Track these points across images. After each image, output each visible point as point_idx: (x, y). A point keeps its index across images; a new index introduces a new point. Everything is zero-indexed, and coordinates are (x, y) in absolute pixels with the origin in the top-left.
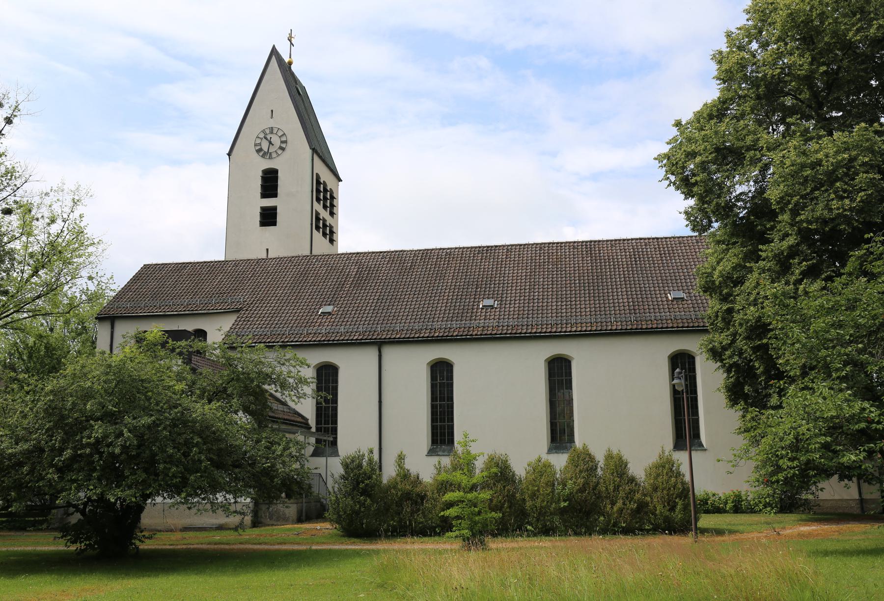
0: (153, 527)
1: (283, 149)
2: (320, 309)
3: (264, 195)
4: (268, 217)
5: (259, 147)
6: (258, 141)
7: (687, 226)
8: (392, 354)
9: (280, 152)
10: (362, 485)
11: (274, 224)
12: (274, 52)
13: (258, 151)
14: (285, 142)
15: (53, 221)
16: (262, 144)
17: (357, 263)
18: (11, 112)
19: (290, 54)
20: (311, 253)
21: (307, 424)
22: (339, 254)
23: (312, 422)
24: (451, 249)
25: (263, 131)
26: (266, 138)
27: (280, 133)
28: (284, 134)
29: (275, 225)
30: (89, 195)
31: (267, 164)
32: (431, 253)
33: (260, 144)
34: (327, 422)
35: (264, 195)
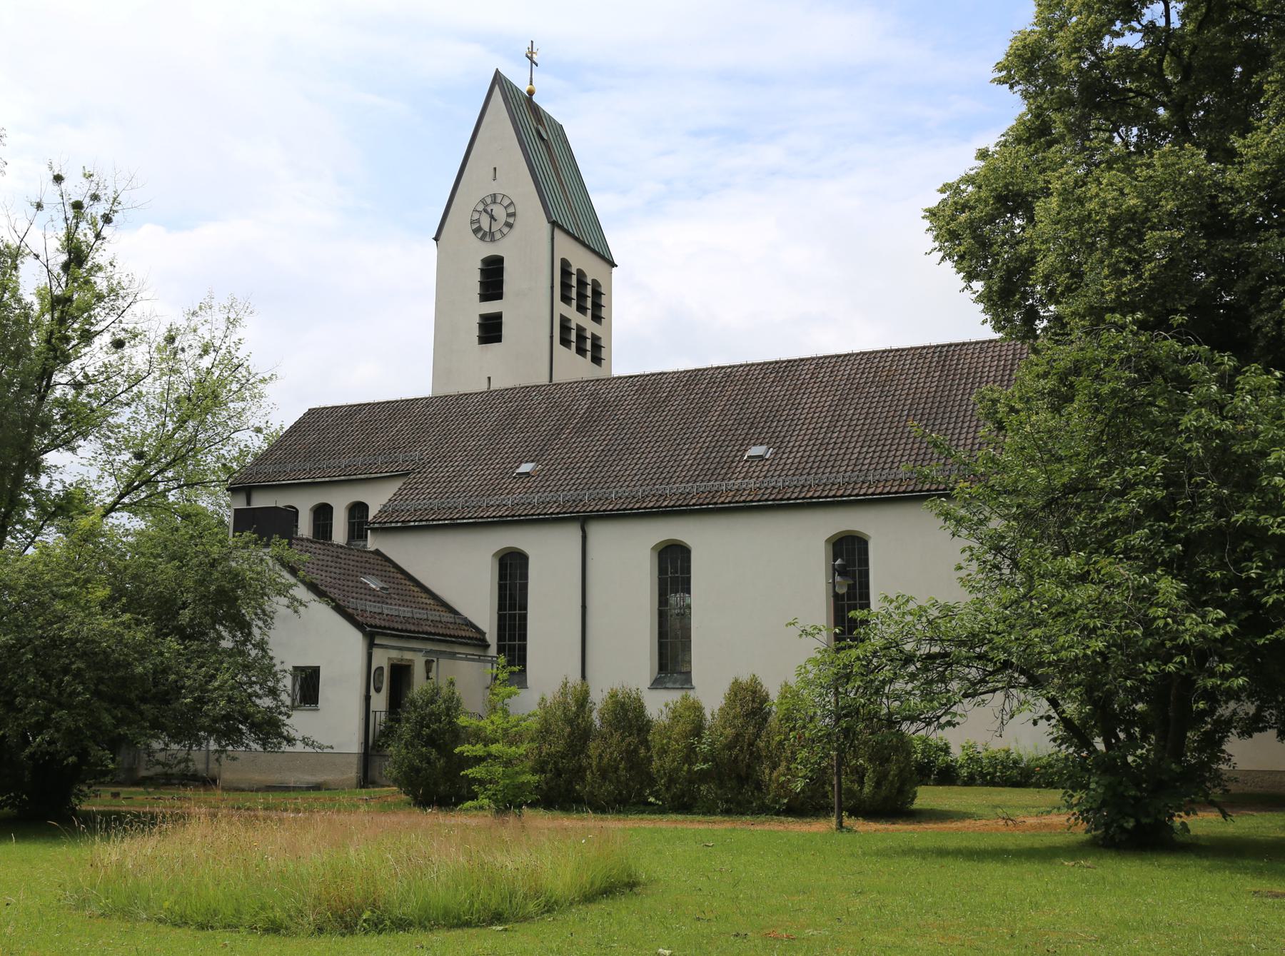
0: (235, 785)
1: (510, 226)
2: (746, 450)
3: (485, 297)
4: (491, 330)
5: (476, 226)
6: (476, 216)
7: (984, 322)
8: (601, 534)
9: (505, 230)
10: (426, 731)
11: (498, 339)
12: (498, 79)
13: (476, 231)
14: (513, 215)
15: (206, 352)
16: (482, 221)
17: (592, 394)
18: (108, 207)
19: (531, 79)
20: (551, 380)
21: (484, 640)
22: (614, 378)
23: (492, 637)
24: (734, 366)
25: (483, 201)
26: (485, 211)
27: (506, 202)
28: (512, 203)
29: (500, 341)
30: (249, 311)
31: (489, 250)
32: (961, 350)
33: (478, 221)
34: (512, 638)
35: (485, 297)
